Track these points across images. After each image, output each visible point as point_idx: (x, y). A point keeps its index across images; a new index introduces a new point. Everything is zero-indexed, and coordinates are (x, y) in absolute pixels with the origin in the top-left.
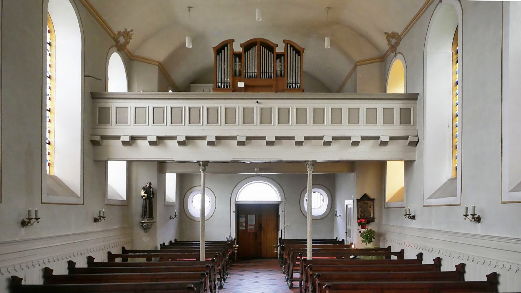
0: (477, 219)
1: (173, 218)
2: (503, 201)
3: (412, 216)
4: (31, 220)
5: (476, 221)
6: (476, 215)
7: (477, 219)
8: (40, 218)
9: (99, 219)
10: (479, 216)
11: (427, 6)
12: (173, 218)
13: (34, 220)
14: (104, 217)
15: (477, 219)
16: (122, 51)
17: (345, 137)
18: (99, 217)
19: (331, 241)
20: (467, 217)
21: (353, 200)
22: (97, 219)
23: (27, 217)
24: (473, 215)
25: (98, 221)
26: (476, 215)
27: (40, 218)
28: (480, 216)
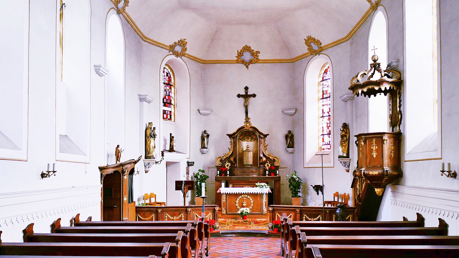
0: (454, 175)
1: (135, 175)
2: (304, 167)
3: (453, 174)
4: (50, 173)
5: (452, 177)
6: (451, 171)
7: (453, 175)
8: (56, 172)
9: (47, 175)
10: (455, 171)
11: (362, 21)
12: (135, 175)
13: (52, 173)
14: (54, 172)
15: (454, 175)
16: (121, 15)
17: (271, 237)
18: (47, 172)
19: (352, 219)
20: (444, 173)
21: (151, 202)
22: (44, 174)
23: (47, 171)
24: (449, 172)
25: (46, 177)
26: (451, 171)
27: (56, 172)
28: (456, 172)
